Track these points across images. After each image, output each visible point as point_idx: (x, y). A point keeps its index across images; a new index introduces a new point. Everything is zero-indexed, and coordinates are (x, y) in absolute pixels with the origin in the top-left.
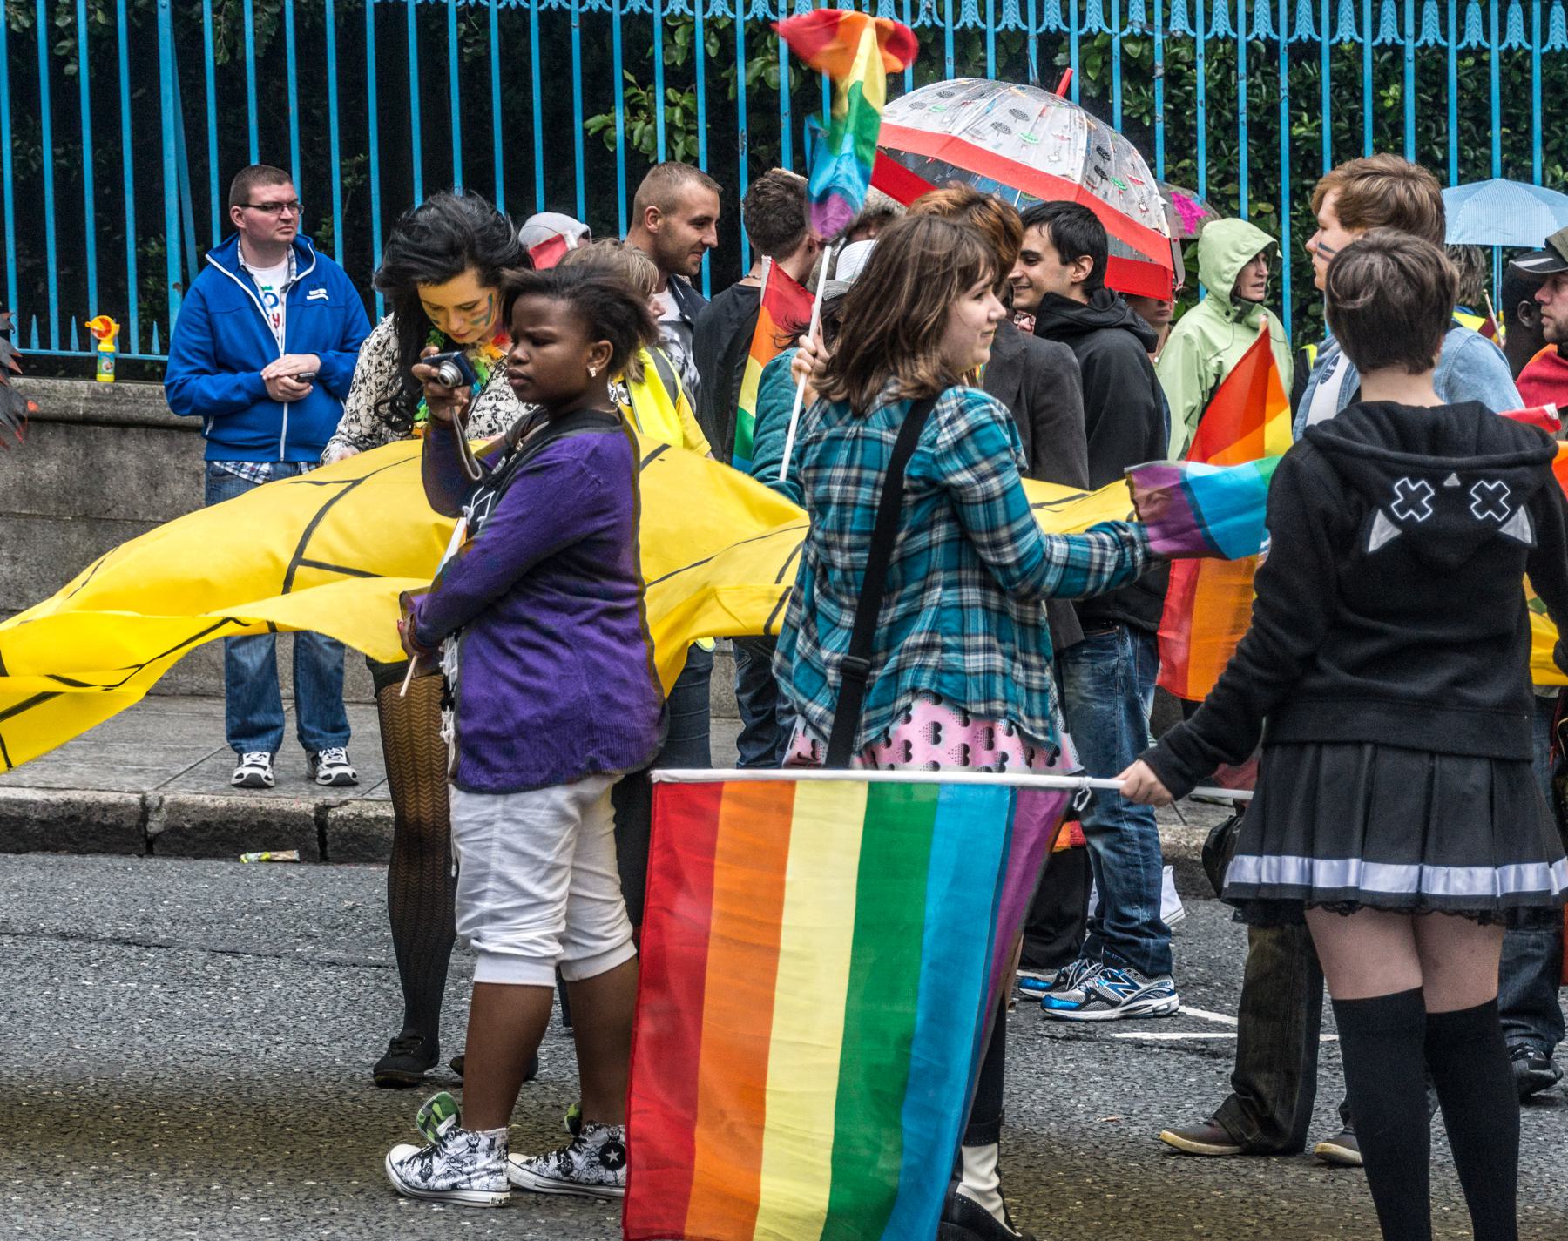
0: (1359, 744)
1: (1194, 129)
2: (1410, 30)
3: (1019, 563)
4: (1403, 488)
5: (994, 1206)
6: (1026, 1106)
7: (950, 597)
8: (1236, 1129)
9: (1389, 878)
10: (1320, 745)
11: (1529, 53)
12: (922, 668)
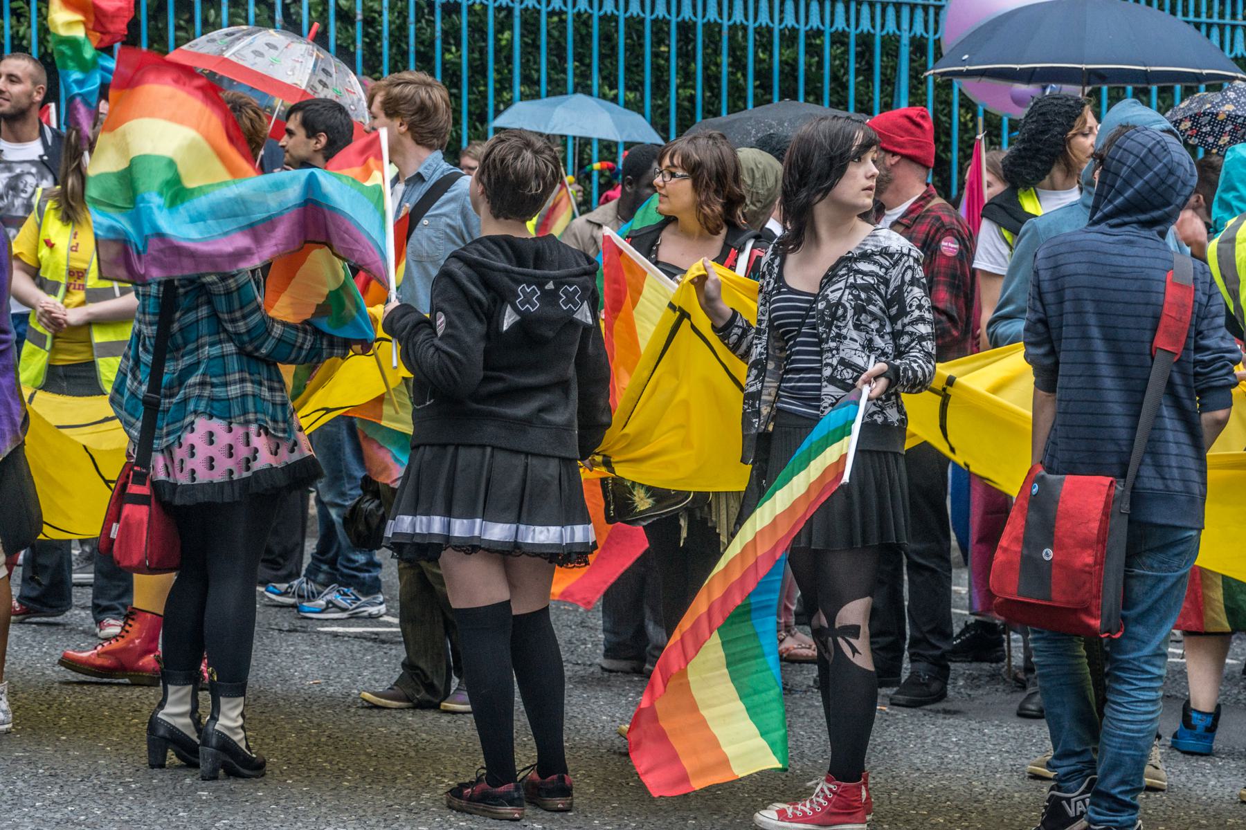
0: (483, 446)
1: (381, 54)
2: (827, 21)
3: (249, 332)
4: (523, 291)
5: (238, 737)
6: (262, 674)
7: (215, 351)
8: (409, 692)
9: (498, 532)
10: (457, 446)
11: (591, 16)
12: (200, 397)
